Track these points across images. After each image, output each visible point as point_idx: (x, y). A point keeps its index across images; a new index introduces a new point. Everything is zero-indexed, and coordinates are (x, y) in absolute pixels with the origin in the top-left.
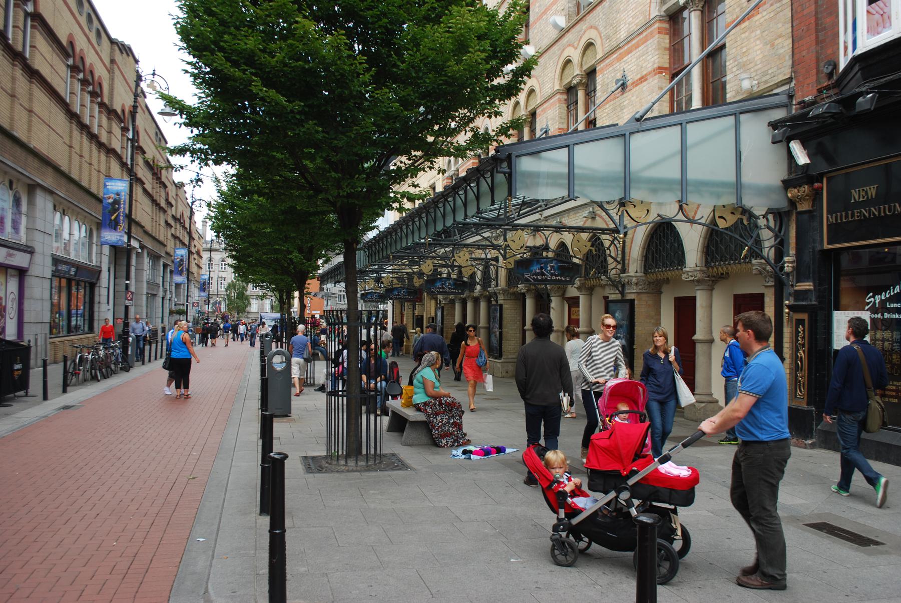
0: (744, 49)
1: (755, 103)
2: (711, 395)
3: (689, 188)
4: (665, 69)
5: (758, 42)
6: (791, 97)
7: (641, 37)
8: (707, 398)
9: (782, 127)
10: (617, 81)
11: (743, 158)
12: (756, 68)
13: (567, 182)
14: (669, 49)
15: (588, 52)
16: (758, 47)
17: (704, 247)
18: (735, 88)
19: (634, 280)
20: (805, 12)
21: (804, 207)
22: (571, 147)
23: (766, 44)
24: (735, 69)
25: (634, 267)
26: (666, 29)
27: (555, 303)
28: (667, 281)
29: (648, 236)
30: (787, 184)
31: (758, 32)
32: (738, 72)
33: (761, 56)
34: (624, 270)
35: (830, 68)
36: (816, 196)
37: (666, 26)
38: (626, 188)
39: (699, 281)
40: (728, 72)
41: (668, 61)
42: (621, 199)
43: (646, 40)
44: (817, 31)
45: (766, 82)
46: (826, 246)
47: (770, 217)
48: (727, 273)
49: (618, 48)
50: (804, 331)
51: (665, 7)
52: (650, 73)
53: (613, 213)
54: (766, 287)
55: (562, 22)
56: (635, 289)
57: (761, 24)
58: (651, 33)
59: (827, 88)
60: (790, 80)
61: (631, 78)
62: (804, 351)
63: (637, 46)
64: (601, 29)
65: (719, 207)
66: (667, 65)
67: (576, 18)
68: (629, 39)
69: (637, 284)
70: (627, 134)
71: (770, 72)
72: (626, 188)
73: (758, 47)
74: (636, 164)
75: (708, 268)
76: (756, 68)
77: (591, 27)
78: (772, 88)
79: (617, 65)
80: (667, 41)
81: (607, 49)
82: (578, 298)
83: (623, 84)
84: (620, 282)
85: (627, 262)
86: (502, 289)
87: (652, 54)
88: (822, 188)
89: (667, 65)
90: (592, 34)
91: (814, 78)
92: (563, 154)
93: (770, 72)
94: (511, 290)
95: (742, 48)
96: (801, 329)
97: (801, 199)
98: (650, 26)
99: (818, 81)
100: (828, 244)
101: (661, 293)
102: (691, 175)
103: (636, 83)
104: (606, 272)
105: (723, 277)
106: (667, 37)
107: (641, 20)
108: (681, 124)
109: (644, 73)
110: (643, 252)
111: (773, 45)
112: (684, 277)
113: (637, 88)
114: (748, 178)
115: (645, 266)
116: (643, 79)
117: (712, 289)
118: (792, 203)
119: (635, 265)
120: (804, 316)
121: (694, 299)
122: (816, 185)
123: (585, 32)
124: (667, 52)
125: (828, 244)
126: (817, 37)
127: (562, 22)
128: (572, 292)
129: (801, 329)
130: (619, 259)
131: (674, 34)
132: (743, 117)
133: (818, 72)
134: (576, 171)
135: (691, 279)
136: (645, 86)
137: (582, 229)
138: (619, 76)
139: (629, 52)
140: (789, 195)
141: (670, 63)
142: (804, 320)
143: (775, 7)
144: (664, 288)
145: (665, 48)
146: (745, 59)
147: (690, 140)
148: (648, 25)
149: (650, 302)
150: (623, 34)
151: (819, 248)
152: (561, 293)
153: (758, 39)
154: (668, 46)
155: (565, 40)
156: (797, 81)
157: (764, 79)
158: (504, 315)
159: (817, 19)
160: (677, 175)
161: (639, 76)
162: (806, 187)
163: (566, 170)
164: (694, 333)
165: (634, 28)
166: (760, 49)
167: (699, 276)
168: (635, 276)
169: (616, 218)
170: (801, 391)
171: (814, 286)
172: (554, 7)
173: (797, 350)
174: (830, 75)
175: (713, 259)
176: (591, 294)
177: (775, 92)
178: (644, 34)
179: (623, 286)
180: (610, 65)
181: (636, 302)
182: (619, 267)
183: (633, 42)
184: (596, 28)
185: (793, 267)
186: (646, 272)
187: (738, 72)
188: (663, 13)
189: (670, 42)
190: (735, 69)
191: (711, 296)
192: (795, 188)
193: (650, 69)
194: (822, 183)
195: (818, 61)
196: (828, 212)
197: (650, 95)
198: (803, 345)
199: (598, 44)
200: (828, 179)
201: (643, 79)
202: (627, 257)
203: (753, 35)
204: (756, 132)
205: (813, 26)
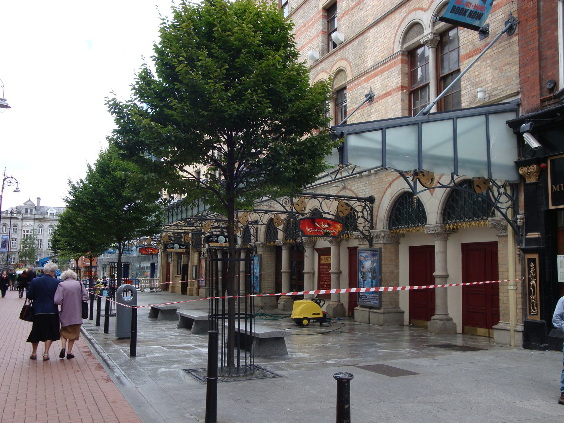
0: (477, 73)
1: (489, 109)
2: (447, 315)
3: (459, 164)
4: (405, 87)
5: (488, 68)
6: (519, 105)
7: (386, 65)
8: (444, 317)
9: (528, 122)
10: (366, 96)
11: (491, 145)
12: (487, 86)
13: (381, 155)
14: (408, 74)
15: (339, 76)
16: (489, 72)
17: (442, 209)
18: (469, 100)
19: (382, 234)
20: (530, 47)
21: (532, 180)
22: (384, 130)
23: (496, 69)
24: (468, 87)
25: (381, 224)
26: (406, 60)
27: (308, 253)
28: (403, 235)
29: (392, 203)
30: (518, 164)
31: (489, 61)
32: (471, 89)
33: (491, 77)
34: (372, 227)
35: (552, 85)
36: (542, 173)
37: (406, 58)
38: (420, 162)
39: (438, 234)
40: (463, 89)
41: (407, 82)
42: (415, 171)
43: (390, 67)
44: (540, 60)
45: (496, 95)
46: (551, 207)
47: (508, 188)
48: (458, 229)
49: (366, 73)
50: (535, 267)
51: (406, 46)
52: (394, 90)
53: (410, 179)
54: (499, 236)
55: (317, 56)
56: (382, 241)
57: (491, 56)
58: (395, 63)
59: (549, 99)
60: (518, 93)
61: (376, 94)
62: (536, 281)
63: (382, 72)
64: (351, 60)
65: (476, 178)
66: (406, 85)
67: (327, 54)
68: (374, 68)
69: (384, 237)
70: (420, 123)
71: (499, 88)
72: (420, 162)
73: (489, 72)
74: (425, 145)
75: (445, 224)
76: (487, 86)
77: (342, 59)
78: (502, 99)
79: (365, 85)
80: (407, 69)
81: (356, 74)
82: (330, 248)
83: (371, 98)
84: (369, 236)
85: (374, 221)
86: (262, 243)
87: (394, 77)
88: (547, 167)
89: (406, 85)
90: (343, 64)
91: (538, 92)
92: (377, 135)
93: (499, 88)
94: (269, 244)
95: (475, 72)
96: (532, 265)
97: (529, 175)
98: (394, 58)
99: (541, 95)
100: (553, 205)
101: (400, 243)
102: (460, 155)
103: (381, 97)
104: (356, 228)
105: (454, 231)
106: (406, 66)
107: (385, 54)
108: (418, 124)
109: (389, 90)
110: (388, 215)
111: (502, 70)
112: (426, 231)
113: (383, 100)
114: (494, 159)
115: (389, 224)
116: (388, 94)
117: (446, 240)
118: (522, 178)
119: (382, 223)
120: (536, 256)
121: (433, 247)
122: (543, 165)
123: (336, 62)
124: (406, 76)
125: (553, 205)
126: (540, 64)
127: (317, 56)
128: (323, 243)
129: (532, 265)
130: (368, 220)
131: (411, 65)
132: (491, 117)
133: (541, 88)
134: (387, 148)
135: (432, 232)
136: (389, 99)
137: (335, 197)
138: (367, 92)
139: (375, 75)
140: (521, 172)
141: (408, 84)
142: (535, 259)
143: (503, 44)
144: (402, 240)
145: (406, 73)
146: (477, 80)
147: (459, 130)
148: (392, 57)
149: (392, 250)
150: (370, 63)
151: (546, 208)
152: (312, 245)
153: (489, 66)
154: (407, 72)
155: (319, 68)
156: (524, 95)
157: (494, 93)
158: (263, 262)
159: (540, 52)
160: (451, 154)
161: (384, 92)
162: (535, 166)
163: (380, 147)
164: (434, 270)
165: (379, 59)
166: (491, 73)
167: (439, 230)
168: (384, 232)
169: (412, 183)
170: (534, 310)
171: (542, 234)
172: (309, 46)
173: (530, 280)
174: (552, 90)
175: (394, 224)
176: (339, 246)
177: (504, 102)
178: (389, 64)
179: (372, 239)
180: (359, 84)
181: (383, 250)
182: (369, 225)
183: (379, 69)
184: (346, 60)
185: (523, 222)
186: (390, 228)
187: (471, 89)
188: (404, 49)
189: (409, 69)
190: (468, 87)
191: (446, 244)
192: (525, 167)
193: (394, 87)
194: (547, 164)
195: (541, 80)
196: (552, 184)
197: (393, 107)
198: (535, 277)
199: (348, 70)
200: (551, 161)
201: (388, 94)
202: (374, 218)
203: (484, 63)
204: (499, 126)
205: (537, 57)
